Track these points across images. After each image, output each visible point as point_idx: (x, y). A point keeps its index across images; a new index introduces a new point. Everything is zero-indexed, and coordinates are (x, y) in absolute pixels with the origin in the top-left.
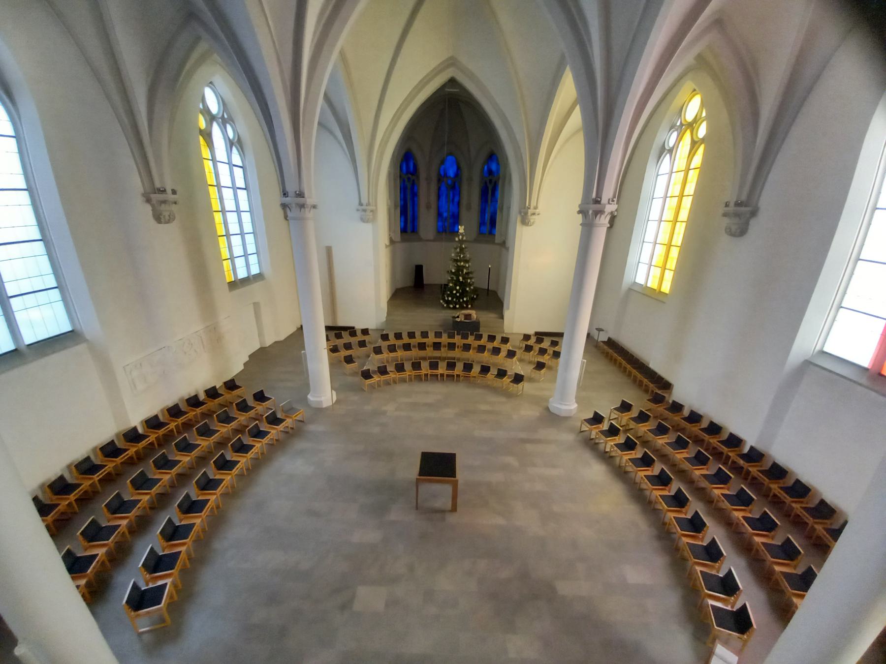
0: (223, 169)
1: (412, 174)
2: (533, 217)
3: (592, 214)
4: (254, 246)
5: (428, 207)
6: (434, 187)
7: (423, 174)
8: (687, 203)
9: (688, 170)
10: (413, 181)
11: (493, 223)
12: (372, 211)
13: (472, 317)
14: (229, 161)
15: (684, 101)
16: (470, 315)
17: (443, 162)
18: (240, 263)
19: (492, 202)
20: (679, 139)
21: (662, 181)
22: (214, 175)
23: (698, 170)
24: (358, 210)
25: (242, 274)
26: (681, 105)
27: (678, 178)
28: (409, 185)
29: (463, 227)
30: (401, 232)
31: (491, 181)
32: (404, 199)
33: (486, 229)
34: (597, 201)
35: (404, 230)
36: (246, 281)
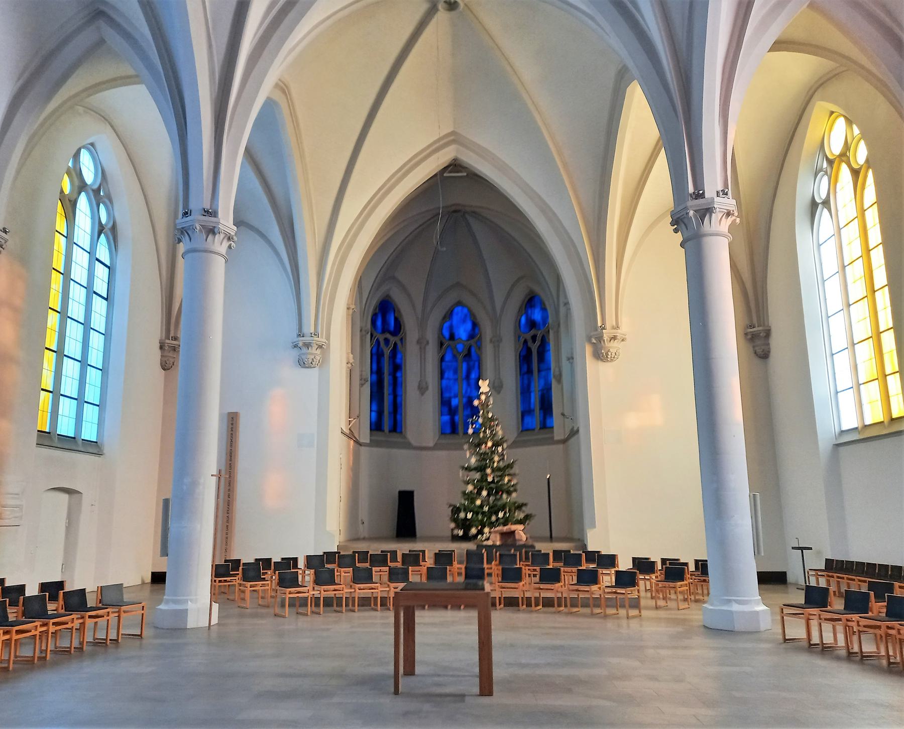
0: (80, 258)
2: (614, 344)
3: (695, 216)
4: (95, 428)
5: (422, 389)
6: (432, 355)
8: (878, 257)
9: (862, 212)
10: (395, 344)
12: (320, 347)
13: (517, 537)
14: (91, 248)
15: (823, 133)
16: (512, 533)
17: (450, 314)
18: (67, 408)
20: (833, 182)
21: (829, 252)
22: (63, 258)
23: (876, 204)
24: (296, 346)
25: (66, 427)
27: (851, 234)
28: (387, 352)
29: (487, 382)
30: (371, 429)
31: (534, 338)
32: (377, 372)
33: (535, 420)
34: (698, 195)
35: (376, 426)
36: (71, 443)
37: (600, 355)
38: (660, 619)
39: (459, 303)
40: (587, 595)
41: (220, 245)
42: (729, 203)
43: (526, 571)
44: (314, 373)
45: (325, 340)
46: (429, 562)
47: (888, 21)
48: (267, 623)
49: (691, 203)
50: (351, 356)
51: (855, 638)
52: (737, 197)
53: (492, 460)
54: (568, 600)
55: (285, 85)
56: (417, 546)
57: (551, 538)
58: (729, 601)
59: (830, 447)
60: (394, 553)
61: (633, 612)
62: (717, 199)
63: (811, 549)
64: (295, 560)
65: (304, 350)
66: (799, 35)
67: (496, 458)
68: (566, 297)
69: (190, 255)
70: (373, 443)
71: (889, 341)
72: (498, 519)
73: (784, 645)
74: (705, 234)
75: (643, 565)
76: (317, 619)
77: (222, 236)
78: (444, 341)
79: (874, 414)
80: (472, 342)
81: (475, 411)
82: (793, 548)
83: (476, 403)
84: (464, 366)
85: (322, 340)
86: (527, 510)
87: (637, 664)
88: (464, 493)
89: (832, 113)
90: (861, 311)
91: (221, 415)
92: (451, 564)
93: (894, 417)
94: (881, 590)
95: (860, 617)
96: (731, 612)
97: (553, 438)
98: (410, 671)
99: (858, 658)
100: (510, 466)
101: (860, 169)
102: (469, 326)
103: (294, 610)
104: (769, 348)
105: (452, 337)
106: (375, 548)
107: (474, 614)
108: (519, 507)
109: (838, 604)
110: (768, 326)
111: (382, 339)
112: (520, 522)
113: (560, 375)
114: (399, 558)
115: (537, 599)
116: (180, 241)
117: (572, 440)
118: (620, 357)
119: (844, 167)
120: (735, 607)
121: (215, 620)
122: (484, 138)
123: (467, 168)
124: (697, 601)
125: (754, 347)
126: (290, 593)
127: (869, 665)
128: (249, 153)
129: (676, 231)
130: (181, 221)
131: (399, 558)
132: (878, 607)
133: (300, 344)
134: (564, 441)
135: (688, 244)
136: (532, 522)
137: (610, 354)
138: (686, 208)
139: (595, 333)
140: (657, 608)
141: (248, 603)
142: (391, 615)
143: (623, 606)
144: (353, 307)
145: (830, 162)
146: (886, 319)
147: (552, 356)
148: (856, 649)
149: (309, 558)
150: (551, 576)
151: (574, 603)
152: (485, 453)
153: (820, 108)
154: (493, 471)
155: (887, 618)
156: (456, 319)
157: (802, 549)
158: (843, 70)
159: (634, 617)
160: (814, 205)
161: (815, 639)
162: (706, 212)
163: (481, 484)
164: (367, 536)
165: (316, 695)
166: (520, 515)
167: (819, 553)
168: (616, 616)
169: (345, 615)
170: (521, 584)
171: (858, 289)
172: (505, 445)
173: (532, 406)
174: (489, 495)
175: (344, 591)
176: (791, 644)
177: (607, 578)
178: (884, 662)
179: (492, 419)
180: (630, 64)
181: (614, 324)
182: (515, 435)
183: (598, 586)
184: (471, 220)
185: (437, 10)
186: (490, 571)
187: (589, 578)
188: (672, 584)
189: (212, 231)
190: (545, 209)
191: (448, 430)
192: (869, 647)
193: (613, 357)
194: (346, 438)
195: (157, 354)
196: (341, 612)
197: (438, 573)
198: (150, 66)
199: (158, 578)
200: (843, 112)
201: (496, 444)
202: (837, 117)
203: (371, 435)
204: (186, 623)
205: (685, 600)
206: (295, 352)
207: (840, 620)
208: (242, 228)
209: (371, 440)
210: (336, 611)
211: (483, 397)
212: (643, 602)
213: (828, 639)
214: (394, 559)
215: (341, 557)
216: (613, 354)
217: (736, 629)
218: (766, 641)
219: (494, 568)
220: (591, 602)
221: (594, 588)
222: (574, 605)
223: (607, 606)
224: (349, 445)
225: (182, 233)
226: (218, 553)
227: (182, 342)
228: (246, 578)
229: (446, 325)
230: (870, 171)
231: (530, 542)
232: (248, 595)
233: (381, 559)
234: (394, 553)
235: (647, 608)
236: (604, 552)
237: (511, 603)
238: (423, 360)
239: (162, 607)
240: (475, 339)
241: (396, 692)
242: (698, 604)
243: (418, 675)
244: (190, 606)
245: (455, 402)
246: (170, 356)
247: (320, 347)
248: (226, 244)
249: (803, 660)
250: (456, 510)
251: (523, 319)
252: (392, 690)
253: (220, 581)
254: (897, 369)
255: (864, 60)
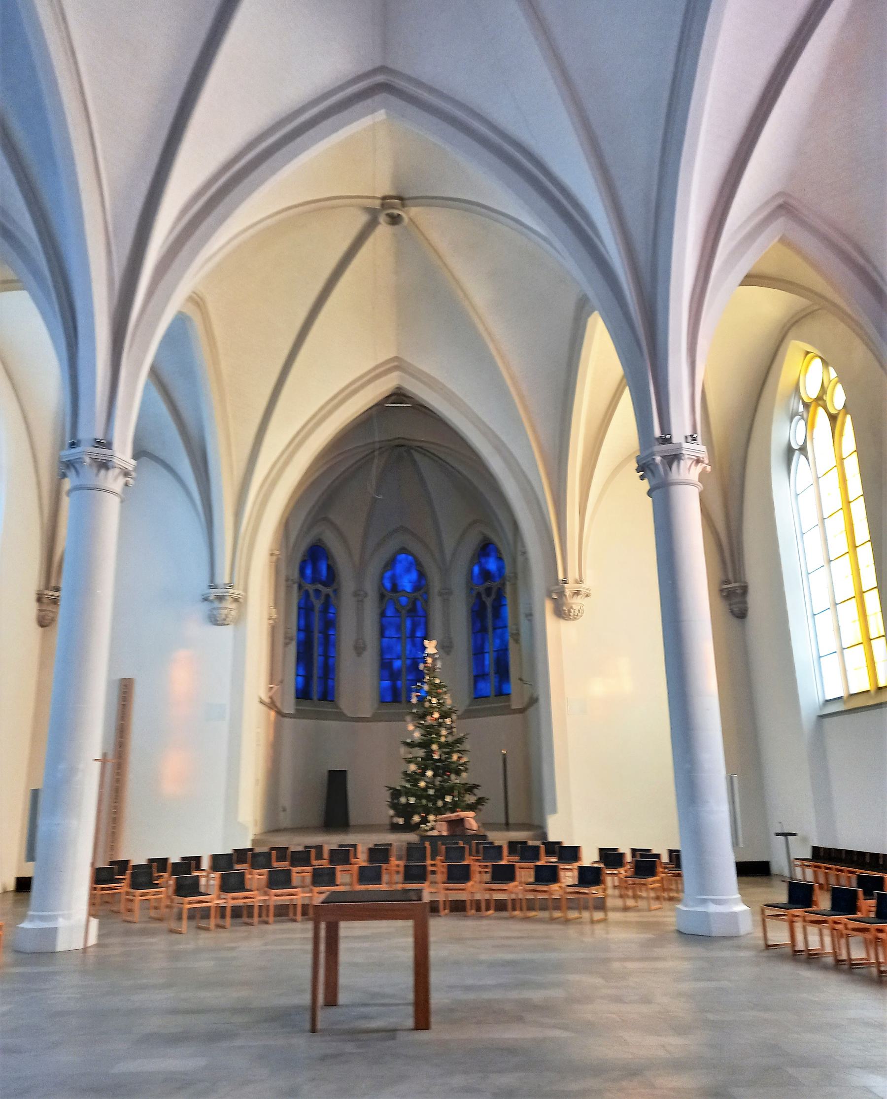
1: (326, 584)
5: (359, 649)
7: (347, 583)
8: (859, 510)
10: (327, 596)
11: (503, 670)
12: (236, 600)
15: (798, 374)
16: (462, 821)
17: (392, 562)
19: (495, 628)
20: (810, 426)
24: (206, 599)
26: (797, 377)
27: (831, 483)
28: (318, 604)
30: (297, 697)
31: (488, 591)
33: (489, 686)
34: (666, 440)
35: (303, 694)
37: (561, 613)
38: (630, 923)
39: (403, 550)
40: (545, 896)
41: (114, 482)
42: (700, 449)
43: (476, 867)
44: (226, 632)
45: (241, 592)
46: (362, 859)
47: (861, 261)
48: (159, 943)
49: (658, 448)
50: (274, 610)
51: (843, 941)
52: (709, 442)
53: (439, 735)
54: (524, 903)
55: (199, 297)
56: (348, 839)
57: (507, 826)
58: (704, 901)
59: (814, 718)
60: (319, 848)
61: (598, 915)
62: (685, 445)
63: (794, 835)
64: (198, 859)
65: (217, 604)
66: (769, 269)
67: (444, 732)
68: (523, 546)
69: (74, 493)
70: (299, 714)
71: (873, 600)
72: (445, 803)
73: (765, 954)
74: (672, 483)
75: (611, 857)
76: (223, 935)
77: (117, 471)
78: (386, 593)
79: (860, 683)
80: (417, 595)
81: (420, 677)
82: (778, 834)
83: (421, 666)
84: (408, 623)
85: (238, 591)
86: (479, 793)
87: (598, 981)
88: (405, 773)
89: (808, 353)
90: (843, 567)
91: (110, 683)
92: (386, 860)
93: (881, 685)
94: (869, 886)
95: (849, 919)
96: (706, 914)
97: (509, 706)
98: (331, 1001)
99: (846, 967)
100: (459, 741)
101: (838, 414)
102: (414, 576)
103: (194, 923)
104: (747, 607)
105: (395, 588)
106: (297, 843)
107: (408, 925)
108: (470, 789)
109: (824, 902)
110: (746, 583)
111: (310, 588)
112: (471, 807)
113: (518, 634)
114: (326, 855)
115: (488, 902)
116: (64, 476)
117: (531, 710)
118: (584, 614)
119: (821, 411)
120: (712, 908)
121: (92, 940)
122: (428, 365)
123: (412, 398)
124: (671, 899)
125: (730, 605)
126: (189, 903)
127: (860, 975)
128: (154, 372)
129: (642, 478)
130: (69, 454)
131: (326, 855)
132: (868, 906)
133: (212, 597)
134: (522, 711)
135: (654, 494)
136: (485, 808)
137: (572, 611)
138: (653, 454)
139: (556, 587)
140: (626, 909)
141: (137, 915)
142: (310, 925)
143: (586, 908)
144: (277, 552)
145: (806, 406)
146: (869, 578)
147: (509, 611)
148: (844, 956)
149: (215, 858)
150: (504, 874)
151: (531, 906)
152: (431, 726)
153: (795, 348)
154: (441, 746)
155: (877, 920)
156: (399, 569)
157: (786, 835)
158: (814, 309)
159: (599, 921)
160: (790, 452)
161: (800, 946)
162: (674, 458)
163: (427, 762)
164: (290, 826)
165: (213, 1037)
166: (470, 799)
167: (805, 840)
168: (577, 921)
169: (257, 929)
170: (470, 884)
171: (839, 544)
172: (454, 717)
173: (486, 670)
174: (434, 776)
175: (257, 898)
176: (773, 951)
177: (569, 876)
178: (874, 970)
179: (439, 686)
180: (591, 294)
181: (577, 577)
182: (467, 702)
183: (559, 884)
184: (417, 456)
185: (379, 223)
186: (433, 869)
187: (548, 875)
188: (643, 881)
189: (104, 465)
190: (500, 448)
191: (389, 698)
192: (858, 954)
193: (576, 614)
194: (263, 708)
195: (31, 609)
196: (251, 924)
197: (369, 875)
198: (35, 273)
199: (23, 885)
200: (816, 352)
201: (444, 715)
202: (813, 358)
203: (297, 704)
204: (54, 945)
205: (658, 898)
206: (205, 606)
207: (825, 922)
208: (144, 459)
209: (297, 710)
210: (247, 924)
211: (429, 660)
212: (610, 902)
213: (814, 943)
214: (319, 856)
215: (255, 855)
216: (577, 612)
217: (713, 935)
218: (747, 948)
219: (438, 865)
220: (550, 904)
221: (554, 887)
222: (531, 908)
223: (570, 908)
224: (269, 715)
225: (68, 466)
226: (101, 850)
227: (62, 594)
228: (135, 885)
229: (388, 574)
230: (849, 417)
231: (483, 832)
232: (136, 906)
233: (301, 858)
234: (319, 848)
235: (615, 909)
236: (566, 844)
237: (458, 907)
238: (360, 611)
239: (26, 925)
240: (422, 591)
241: (313, 1030)
242: (671, 903)
243: (342, 1006)
244: (61, 923)
245: (397, 664)
246: (49, 611)
247: (236, 600)
248: (121, 481)
249: (787, 970)
250: (396, 793)
251: (476, 569)
252: (308, 1026)
253: (103, 889)
254: (883, 633)
255: (839, 301)
